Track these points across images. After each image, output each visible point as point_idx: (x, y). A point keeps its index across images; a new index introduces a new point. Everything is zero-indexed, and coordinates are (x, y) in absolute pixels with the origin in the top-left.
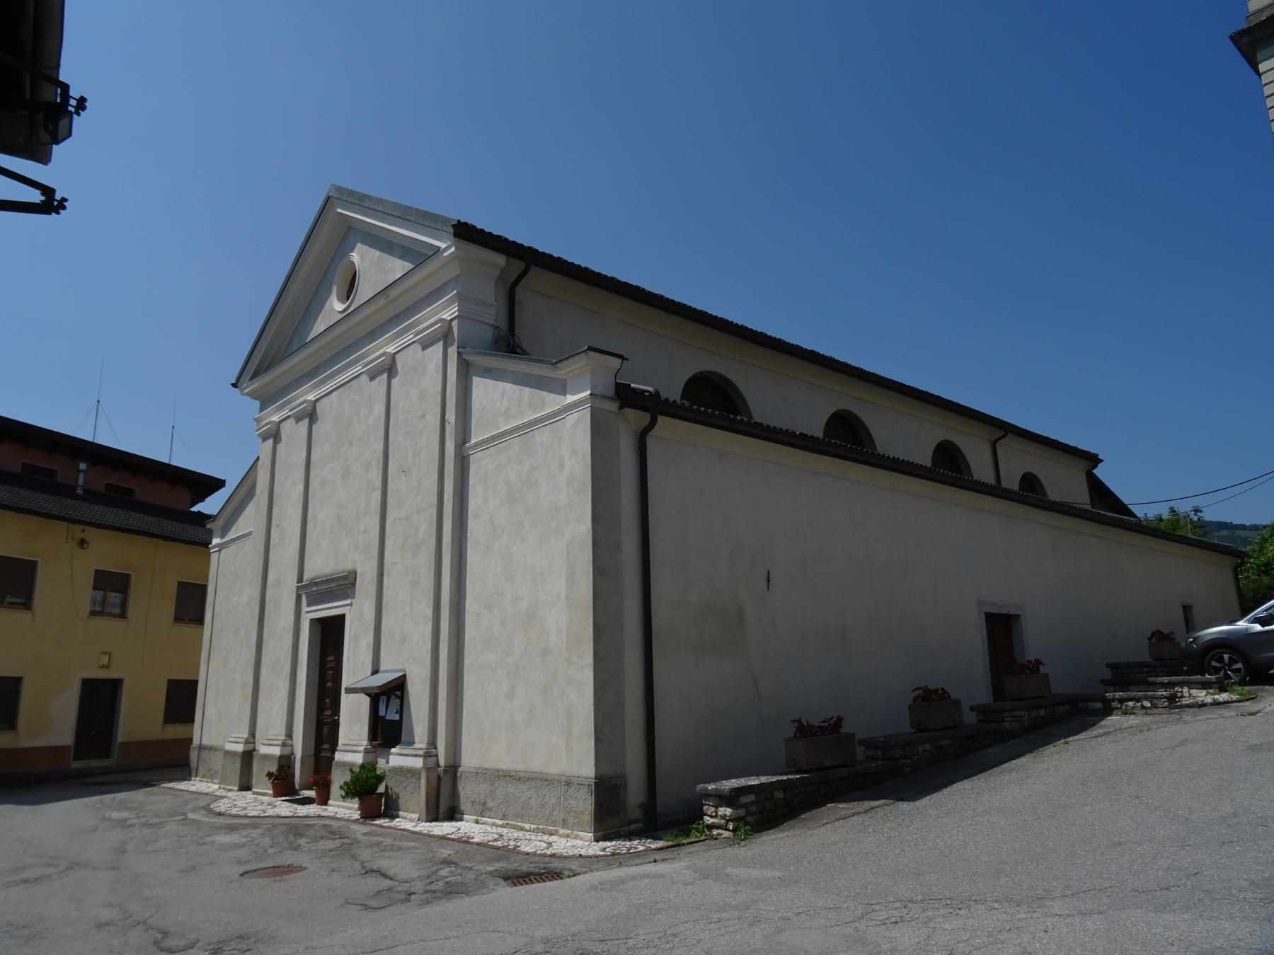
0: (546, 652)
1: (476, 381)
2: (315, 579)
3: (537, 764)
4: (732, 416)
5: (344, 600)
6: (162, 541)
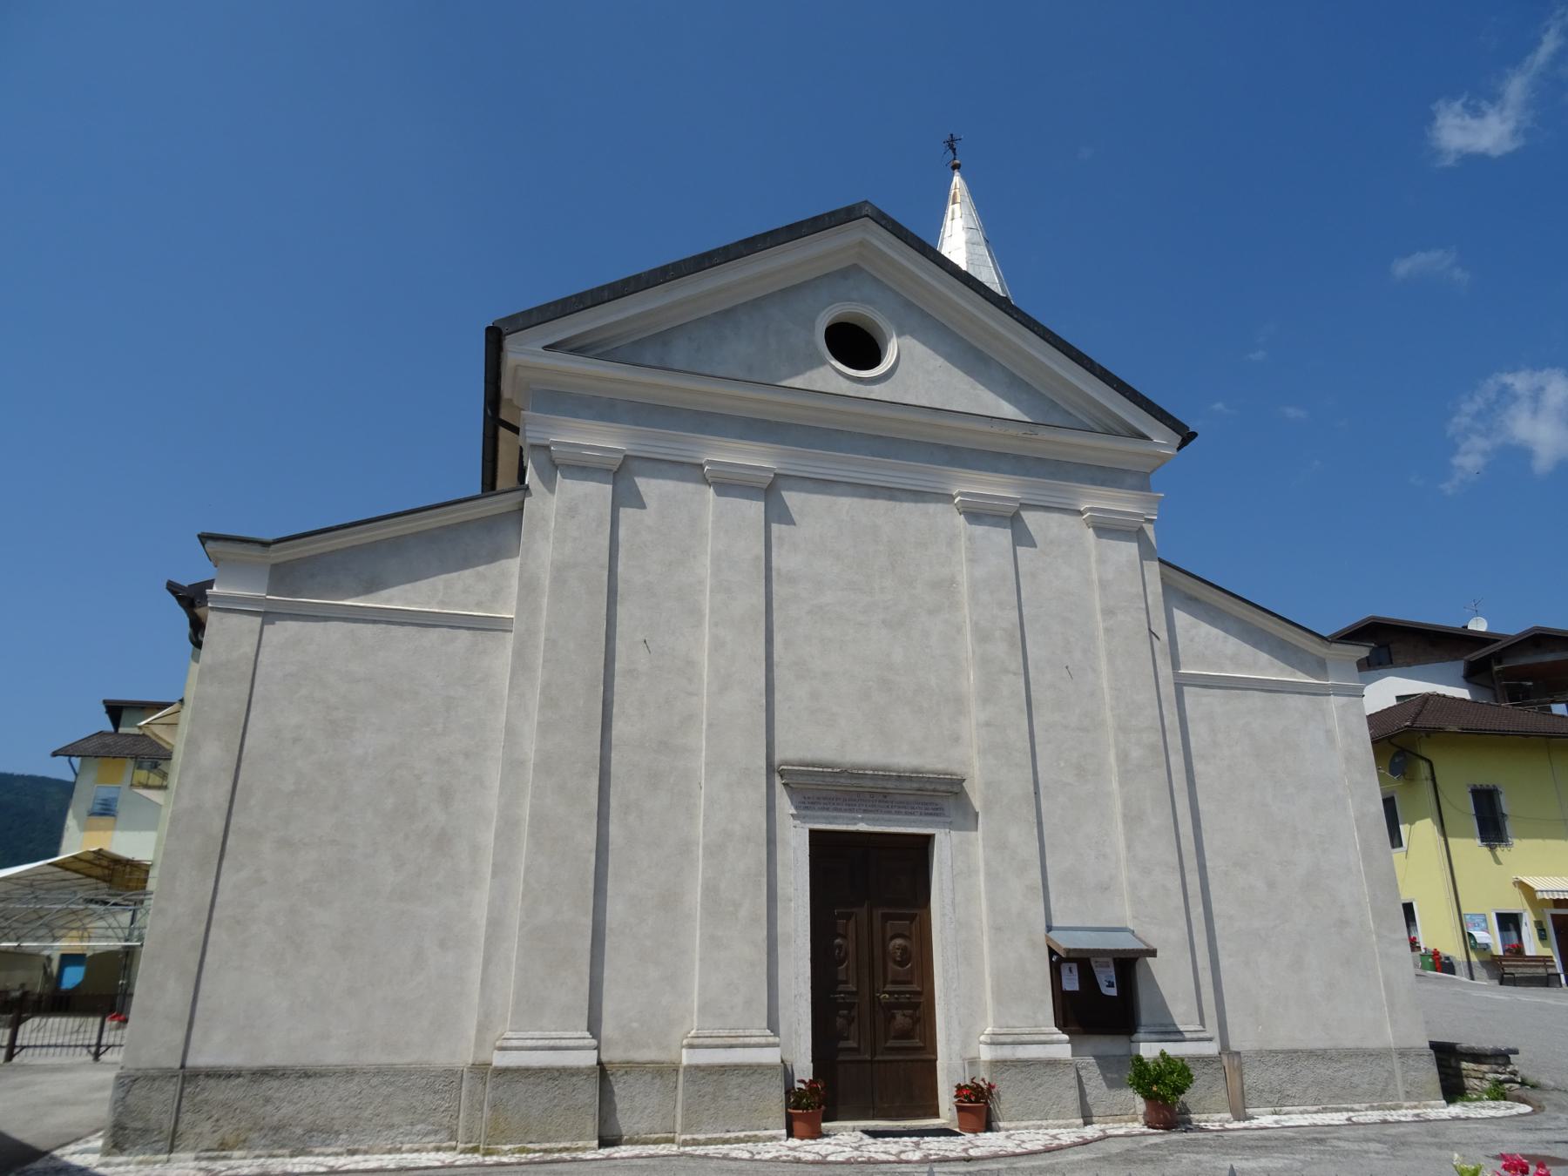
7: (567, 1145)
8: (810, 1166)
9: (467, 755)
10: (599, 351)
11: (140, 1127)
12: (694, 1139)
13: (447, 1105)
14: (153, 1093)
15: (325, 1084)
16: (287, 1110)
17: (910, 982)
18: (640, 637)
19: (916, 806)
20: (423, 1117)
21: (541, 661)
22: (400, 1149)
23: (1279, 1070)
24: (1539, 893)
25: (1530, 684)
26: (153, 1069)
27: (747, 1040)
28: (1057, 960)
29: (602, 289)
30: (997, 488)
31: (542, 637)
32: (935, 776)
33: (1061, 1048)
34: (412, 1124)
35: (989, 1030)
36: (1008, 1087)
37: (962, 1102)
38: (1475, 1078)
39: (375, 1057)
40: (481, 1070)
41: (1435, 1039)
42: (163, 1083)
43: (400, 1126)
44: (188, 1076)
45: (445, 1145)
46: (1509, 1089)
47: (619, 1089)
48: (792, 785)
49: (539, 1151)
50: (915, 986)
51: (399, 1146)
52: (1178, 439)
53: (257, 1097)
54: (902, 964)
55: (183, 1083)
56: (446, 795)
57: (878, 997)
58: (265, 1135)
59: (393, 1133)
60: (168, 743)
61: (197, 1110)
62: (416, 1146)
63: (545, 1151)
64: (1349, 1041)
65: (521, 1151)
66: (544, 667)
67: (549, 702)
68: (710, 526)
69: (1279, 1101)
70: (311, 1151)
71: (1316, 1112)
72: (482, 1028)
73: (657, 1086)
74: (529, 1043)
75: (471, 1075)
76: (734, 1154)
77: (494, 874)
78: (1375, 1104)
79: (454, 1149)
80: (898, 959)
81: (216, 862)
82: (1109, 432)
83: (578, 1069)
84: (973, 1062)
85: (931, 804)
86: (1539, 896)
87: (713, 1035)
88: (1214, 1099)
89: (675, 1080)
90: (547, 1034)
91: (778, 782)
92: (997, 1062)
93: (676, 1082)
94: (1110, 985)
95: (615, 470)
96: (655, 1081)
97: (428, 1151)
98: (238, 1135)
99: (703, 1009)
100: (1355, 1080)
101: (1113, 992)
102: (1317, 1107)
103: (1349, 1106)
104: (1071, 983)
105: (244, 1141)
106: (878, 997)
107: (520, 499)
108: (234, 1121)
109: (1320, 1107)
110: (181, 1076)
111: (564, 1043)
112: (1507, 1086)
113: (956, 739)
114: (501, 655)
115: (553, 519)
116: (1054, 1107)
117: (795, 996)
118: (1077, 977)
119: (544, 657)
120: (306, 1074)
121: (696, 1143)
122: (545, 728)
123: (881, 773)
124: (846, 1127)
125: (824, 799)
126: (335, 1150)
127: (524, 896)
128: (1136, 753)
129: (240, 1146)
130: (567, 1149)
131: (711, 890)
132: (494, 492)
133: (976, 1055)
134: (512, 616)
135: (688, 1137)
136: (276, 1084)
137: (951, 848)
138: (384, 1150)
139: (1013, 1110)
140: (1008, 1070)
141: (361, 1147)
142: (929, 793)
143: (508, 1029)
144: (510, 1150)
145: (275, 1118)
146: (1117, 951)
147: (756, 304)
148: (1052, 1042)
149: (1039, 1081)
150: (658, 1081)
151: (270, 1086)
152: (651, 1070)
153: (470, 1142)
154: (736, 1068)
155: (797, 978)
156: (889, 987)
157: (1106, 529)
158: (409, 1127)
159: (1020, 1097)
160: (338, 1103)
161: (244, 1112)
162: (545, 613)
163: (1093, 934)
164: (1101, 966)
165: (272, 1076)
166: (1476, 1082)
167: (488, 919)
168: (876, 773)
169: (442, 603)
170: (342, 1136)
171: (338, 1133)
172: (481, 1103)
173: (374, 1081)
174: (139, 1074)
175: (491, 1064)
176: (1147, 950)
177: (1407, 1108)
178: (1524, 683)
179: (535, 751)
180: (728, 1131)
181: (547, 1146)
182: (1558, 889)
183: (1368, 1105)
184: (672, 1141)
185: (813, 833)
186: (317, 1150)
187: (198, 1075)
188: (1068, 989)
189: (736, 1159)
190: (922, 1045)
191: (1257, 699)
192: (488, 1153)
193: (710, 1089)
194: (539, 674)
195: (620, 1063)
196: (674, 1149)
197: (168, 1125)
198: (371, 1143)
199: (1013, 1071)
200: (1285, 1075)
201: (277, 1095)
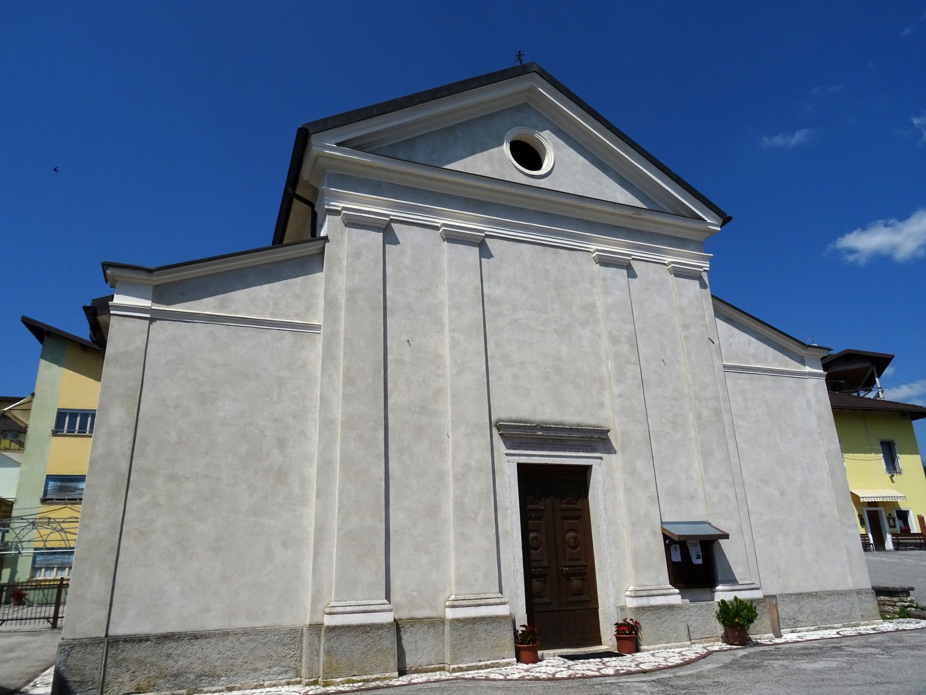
0: (822, 515)
1: (387, 245)
2: (547, 424)
3: (830, 585)
4: (855, 394)
5: (532, 450)
6: (900, 402)
7: (378, 676)
8: (549, 682)
9: (295, 417)
10: (371, 149)
11: (79, 680)
12: (459, 667)
13: (293, 653)
14: (87, 655)
15: (209, 643)
16: (183, 662)
17: (579, 559)
18: (405, 338)
19: (580, 447)
20: (277, 662)
21: (342, 353)
22: (263, 685)
23: (793, 606)
24: (862, 498)
25: (843, 381)
26: (86, 638)
27: (488, 601)
28: (669, 541)
29: (372, 107)
30: (616, 247)
31: (342, 337)
32: (593, 428)
33: (675, 598)
34: (270, 667)
35: (631, 588)
36: (647, 624)
37: (619, 634)
38: (889, 605)
39: (242, 623)
40: (316, 628)
41: (875, 585)
42: (94, 648)
43: (262, 669)
44: (112, 642)
45: (293, 680)
46: (910, 611)
47: (405, 637)
48: (505, 435)
49: (360, 681)
50: (583, 562)
51: (262, 683)
52: (721, 221)
53: (162, 654)
54: (574, 548)
55: (107, 648)
56: (282, 444)
57: (562, 570)
58: (169, 680)
59: (257, 675)
60: (23, 422)
61: (118, 664)
62: (274, 682)
63: (364, 681)
64: (830, 587)
65: (349, 682)
66: (344, 357)
67: (349, 381)
68: (445, 267)
69: (794, 626)
70: (201, 690)
71: (814, 630)
72: (315, 600)
73: (431, 634)
74: (349, 609)
75: (310, 632)
76: (492, 676)
77: (318, 496)
78: (846, 624)
79: (299, 683)
80: (572, 545)
81: (125, 491)
82: (678, 215)
83: (382, 624)
84: (622, 609)
85: (590, 446)
86: (862, 500)
87: (466, 598)
88: (763, 625)
89: (442, 629)
90: (359, 602)
91: (495, 431)
92: (640, 608)
93: (443, 630)
94: (698, 557)
95: (384, 228)
96: (430, 630)
97: (282, 685)
98: (149, 682)
99: (459, 582)
100: (834, 609)
101: (700, 561)
102: (815, 627)
103: (832, 626)
104: (677, 557)
105: (154, 686)
106: (562, 570)
107: (322, 246)
108: (146, 672)
109: (817, 627)
110: (106, 643)
111: (372, 608)
112: (909, 609)
113: (602, 405)
114: (315, 350)
115: (346, 260)
116: (674, 634)
117: (514, 571)
118: (679, 553)
119: (344, 351)
120: (195, 637)
121: (461, 670)
122: (347, 398)
123: (560, 426)
124: (549, 654)
125: (525, 443)
126: (218, 688)
127: (339, 510)
128: (706, 413)
129: (151, 688)
130: (378, 679)
131: (459, 504)
132: (281, 245)
133: (623, 604)
134: (320, 324)
135: (456, 666)
136: (174, 644)
137: (602, 473)
138: (252, 687)
139: (650, 638)
140: (646, 613)
141: (236, 685)
142: (588, 439)
143: (333, 600)
144: (341, 681)
145: (175, 669)
146: (700, 536)
147: (466, 124)
148: (670, 594)
149: (664, 619)
150: (432, 631)
151: (170, 646)
152: (427, 623)
153: (312, 678)
154: (483, 619)
155: (514, 559)
156: (568, 563)
157: (680, 273)
158: (268, 670)
159: (654, 629)
160: (218, 656)
161: (153, 665)
162: (343, 321)
163: (687, 526)
164: (692, 546)
165: (172, 639)
166: (891, 608)
167: (315, 526)
168: (557, 426)
169: (273, 314)
170: (222, 679)
171: (219, 677)
172: (318, 651)
173: (243, 639)
174: (76, 642)
175: (323, 624)
176: (724, 535)
177: (863, 625)
178: (840, 381)
179: (342, 413)
180: (480, 661)
181: (365, 677)
182: (872, 496)
183: (842, 624)
184: (443, 669)
185: (520, 466)
186: (206, 689)
187: (119, 641)
188: (675, 560)
189: (495, 680)
190: (589, 599)
191: (768, 380)
192: (326, 685)
193: (467, 634)
194: (341, 362)
195: (406, 620)
196: (445, 675)
197: (98, 676)
198: (242, 682)
199: (649, 613)
200: (796, 608)
201: (175, 652)
